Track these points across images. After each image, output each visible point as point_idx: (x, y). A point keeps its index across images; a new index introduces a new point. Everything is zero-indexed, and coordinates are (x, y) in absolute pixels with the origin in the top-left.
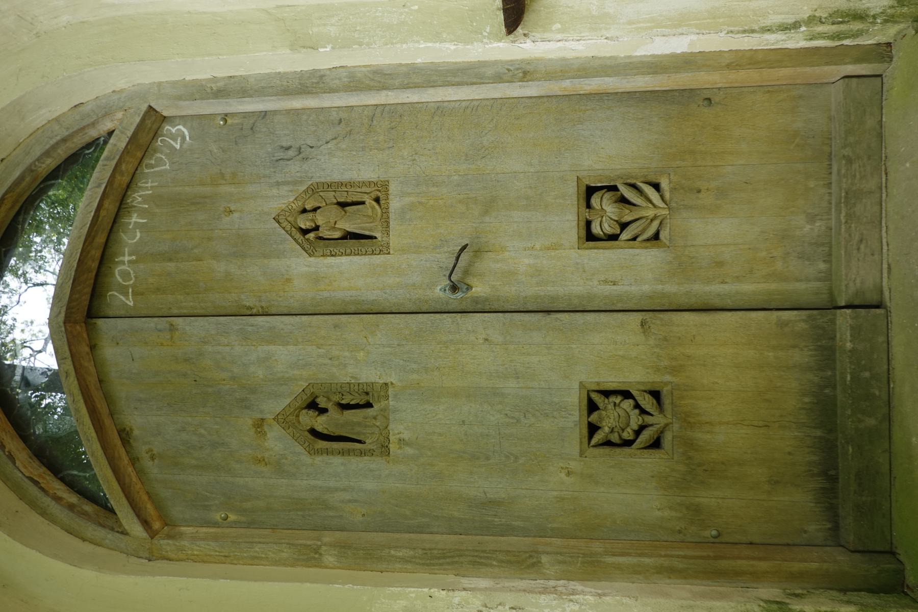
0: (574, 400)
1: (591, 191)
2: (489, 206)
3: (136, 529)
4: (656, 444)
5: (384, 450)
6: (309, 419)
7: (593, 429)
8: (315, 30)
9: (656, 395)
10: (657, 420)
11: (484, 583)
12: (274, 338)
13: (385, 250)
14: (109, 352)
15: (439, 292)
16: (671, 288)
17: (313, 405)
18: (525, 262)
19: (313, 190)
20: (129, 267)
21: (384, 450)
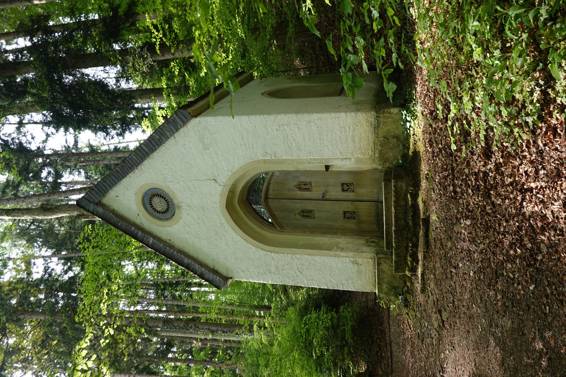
0: (342, 212)
1: (343, 184)
2: (328, 186)
3: (279, 228)
4: (354, 218)
5: (314, 218)
6: (302, 214)
7: (345, 216)
8: (410, 154)
9: (354, 212)
10: (354, 216)
11: (329, 236)
12: (296, 203)
13: (312, 191)
14: (270, 204)
15: (321, 197)
16: (356, 198)
17: (303, 212)
18: (334, 193)
19: (300, 182)
20: (49, 222)
21: (314, 218)
